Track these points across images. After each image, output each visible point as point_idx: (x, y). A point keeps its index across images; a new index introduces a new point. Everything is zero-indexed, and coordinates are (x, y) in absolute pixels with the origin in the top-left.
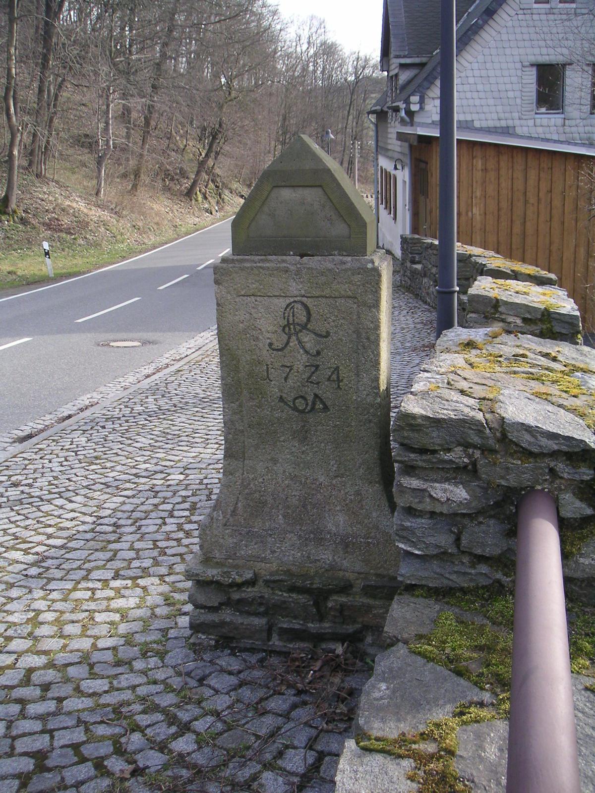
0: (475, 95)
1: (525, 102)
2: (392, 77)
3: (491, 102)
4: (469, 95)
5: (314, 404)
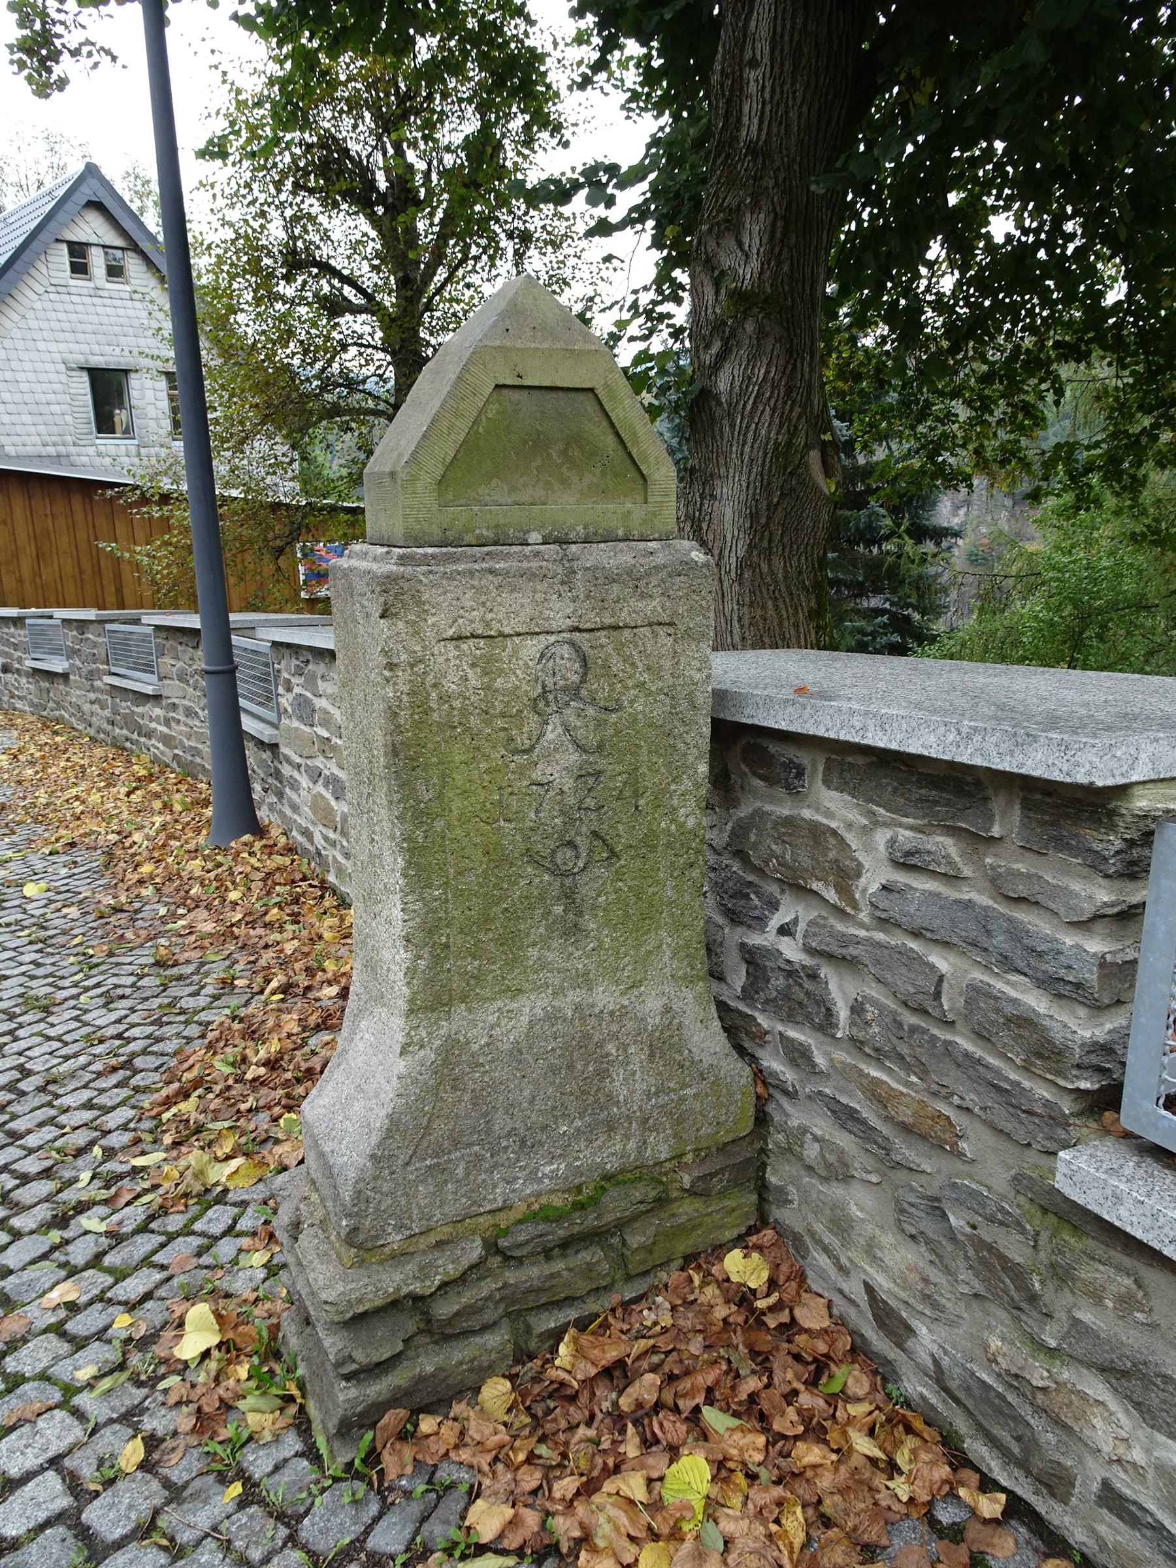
3: (28, 419)
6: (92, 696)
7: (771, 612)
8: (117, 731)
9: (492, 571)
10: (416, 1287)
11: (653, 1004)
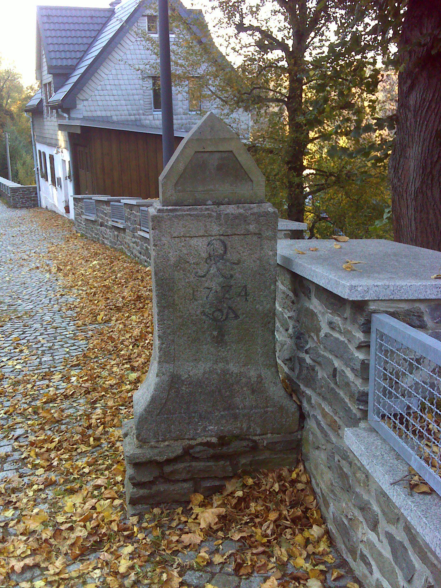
0: (112, 98)
1: (146, 103)
2: (45, 85)
3: (123, 102)
4: (107, 98)
5: (228, 314)
6: (134, 240)
7: (431, 216)
8: (142, 257)
9: (191, 215)
10: (158, 458)
11: (252, 373)
